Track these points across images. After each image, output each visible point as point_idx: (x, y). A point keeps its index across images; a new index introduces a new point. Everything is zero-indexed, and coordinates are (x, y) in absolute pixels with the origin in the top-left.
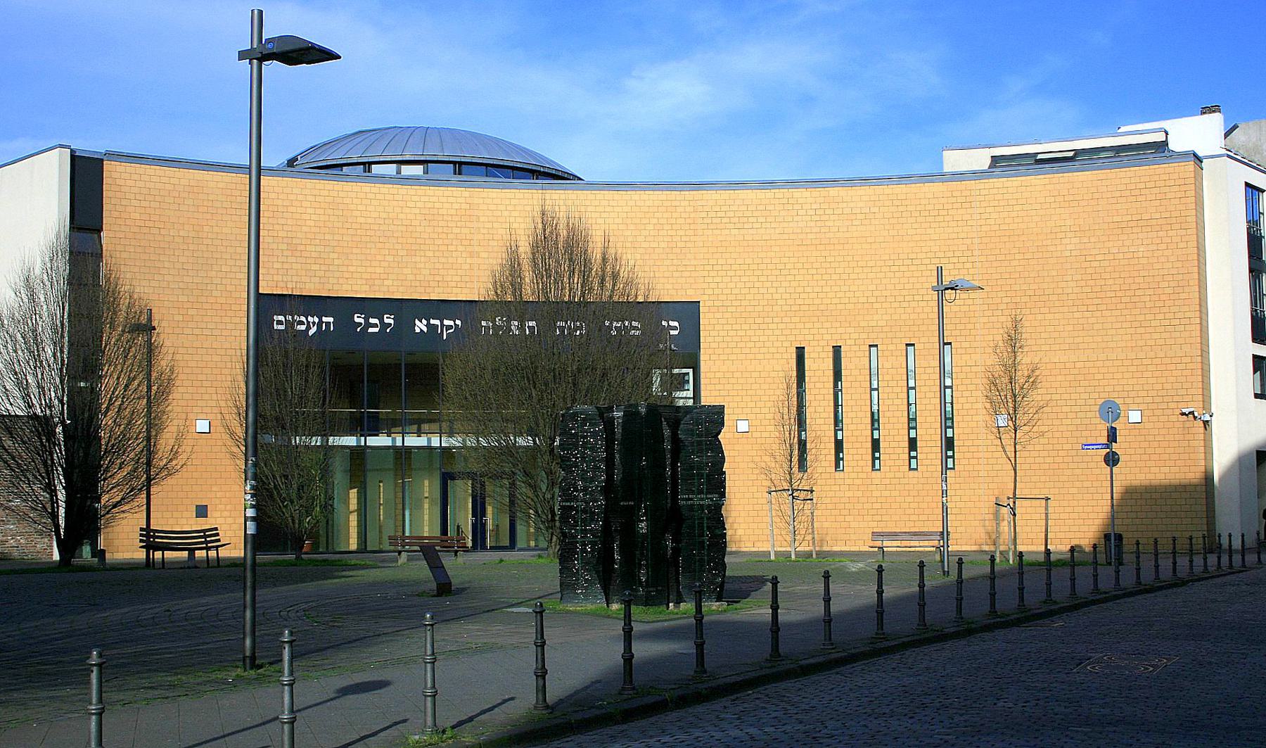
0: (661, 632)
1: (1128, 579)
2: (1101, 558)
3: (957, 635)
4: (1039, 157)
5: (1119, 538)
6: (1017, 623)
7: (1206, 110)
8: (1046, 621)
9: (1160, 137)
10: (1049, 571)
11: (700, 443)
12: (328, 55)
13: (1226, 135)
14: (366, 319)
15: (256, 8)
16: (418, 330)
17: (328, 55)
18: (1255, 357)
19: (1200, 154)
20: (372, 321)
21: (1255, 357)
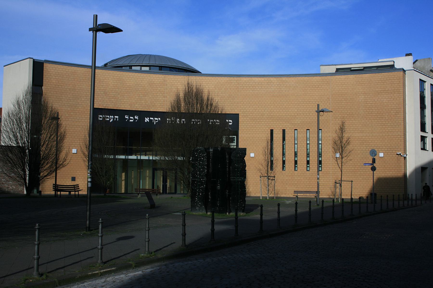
4: (352, 69)
5: (375, 194)
7: (407, 55)
9: (392, 63)
13: (414, 63)
14: (129, 117)
16: (146, 121)
18: (421, 136)
20: (131, 118)
21: (421, 136)
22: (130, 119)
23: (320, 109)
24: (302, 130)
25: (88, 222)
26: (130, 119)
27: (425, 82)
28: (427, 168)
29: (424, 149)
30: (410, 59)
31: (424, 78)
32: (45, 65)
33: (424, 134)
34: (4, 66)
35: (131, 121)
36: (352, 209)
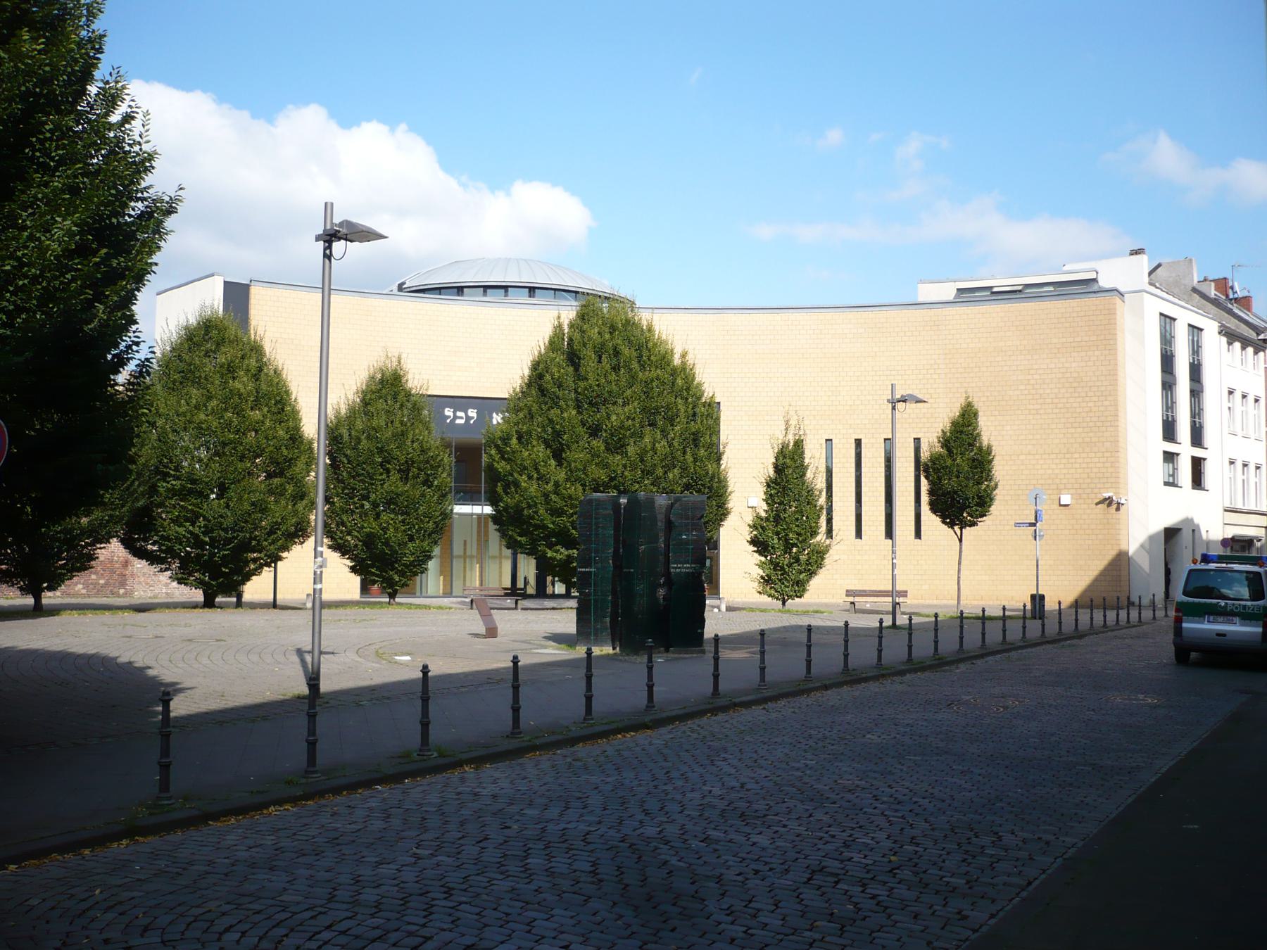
0: (623, 678)
1: (1052, 629)
2: (1029, 615)
3: (876, 678)
4: (995, 290)
5: (1042, 597)
6: (930, 668)
7: (1135, 252)
8: (953, 667)
9: (1093, 276)
10: (983, 624)
11: (687, 525)
12: (382, 237)
13: (1150, 273)
14: (454, 413)
15: (329, 201)
16: (495, 422)
17: (382, 237)
18: (1165, 452)
19: (1122, 290)
20: (459, 414)
21: (1165, 452)
22: (455, 417)
23: (898, 396)
24: (873, 441)
25: (1237, 567)
26: (455, 417)
27: (1175, 320)
28: (1179, 530)
29: (1171, 483)
30: (1144, 263)
31: (1171, 310)
32: (254, 291)
33: (1171, 447)
34: (158, 294)
35: (458, 421)
36: (961, 638)
